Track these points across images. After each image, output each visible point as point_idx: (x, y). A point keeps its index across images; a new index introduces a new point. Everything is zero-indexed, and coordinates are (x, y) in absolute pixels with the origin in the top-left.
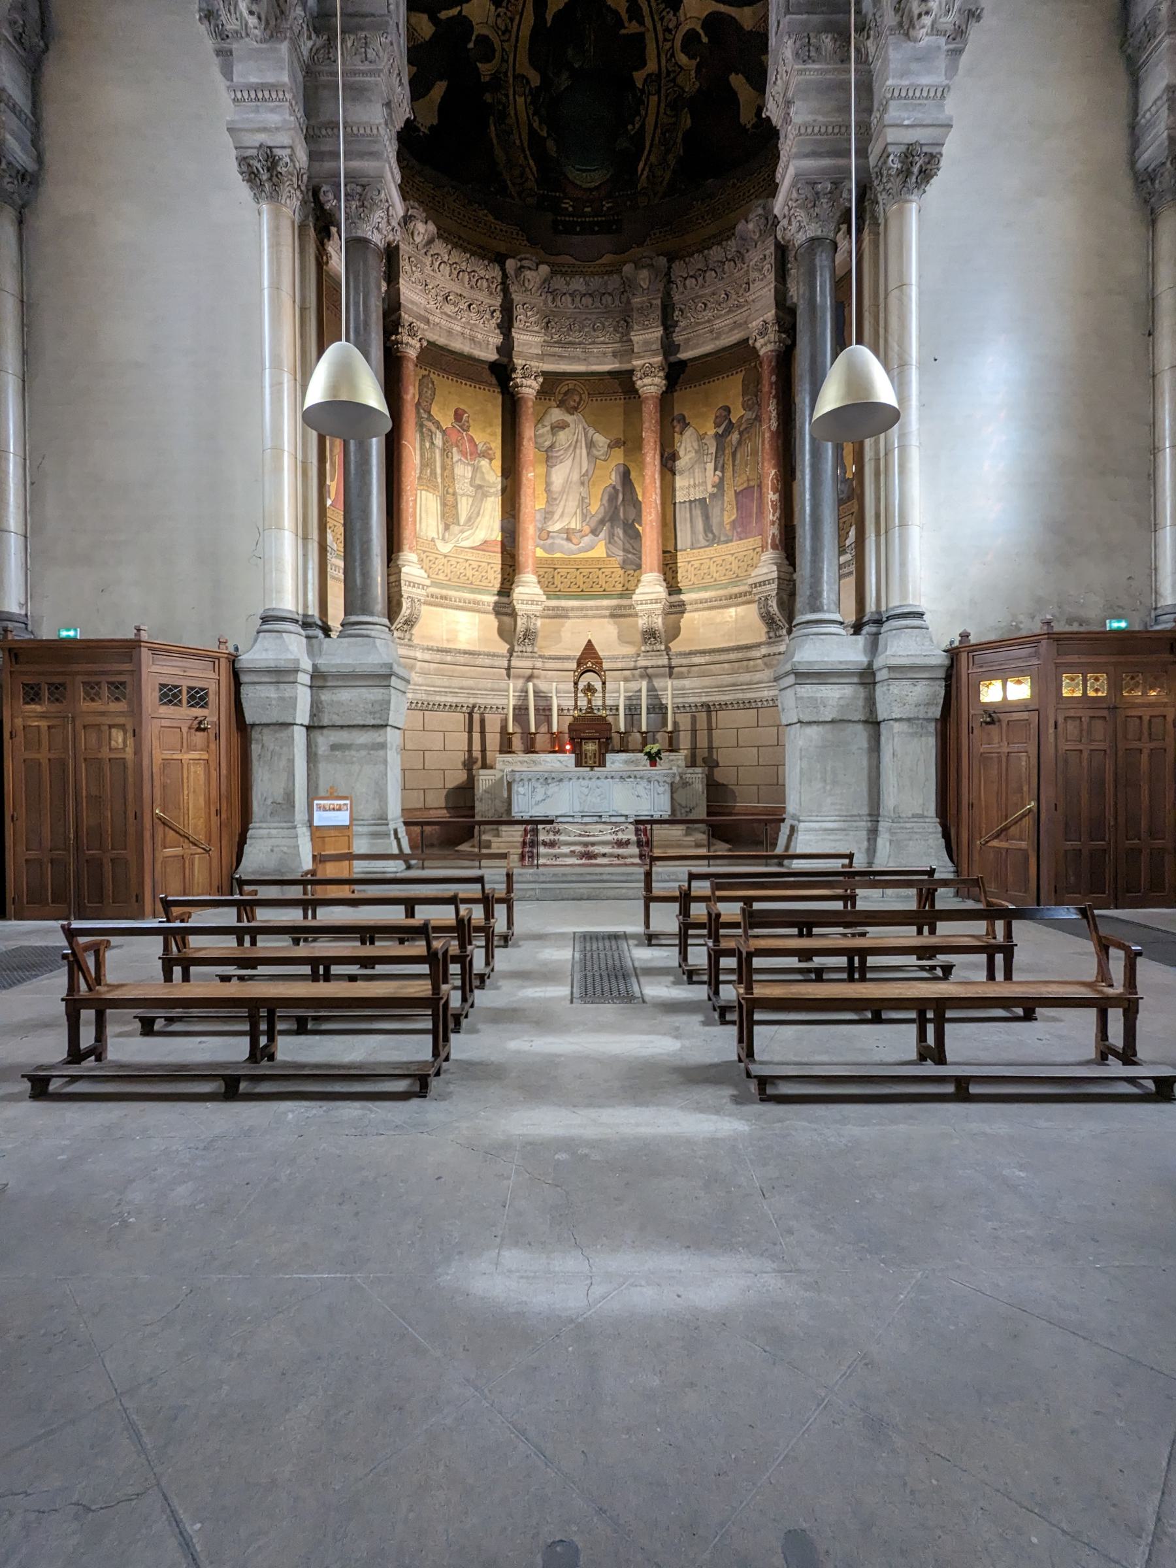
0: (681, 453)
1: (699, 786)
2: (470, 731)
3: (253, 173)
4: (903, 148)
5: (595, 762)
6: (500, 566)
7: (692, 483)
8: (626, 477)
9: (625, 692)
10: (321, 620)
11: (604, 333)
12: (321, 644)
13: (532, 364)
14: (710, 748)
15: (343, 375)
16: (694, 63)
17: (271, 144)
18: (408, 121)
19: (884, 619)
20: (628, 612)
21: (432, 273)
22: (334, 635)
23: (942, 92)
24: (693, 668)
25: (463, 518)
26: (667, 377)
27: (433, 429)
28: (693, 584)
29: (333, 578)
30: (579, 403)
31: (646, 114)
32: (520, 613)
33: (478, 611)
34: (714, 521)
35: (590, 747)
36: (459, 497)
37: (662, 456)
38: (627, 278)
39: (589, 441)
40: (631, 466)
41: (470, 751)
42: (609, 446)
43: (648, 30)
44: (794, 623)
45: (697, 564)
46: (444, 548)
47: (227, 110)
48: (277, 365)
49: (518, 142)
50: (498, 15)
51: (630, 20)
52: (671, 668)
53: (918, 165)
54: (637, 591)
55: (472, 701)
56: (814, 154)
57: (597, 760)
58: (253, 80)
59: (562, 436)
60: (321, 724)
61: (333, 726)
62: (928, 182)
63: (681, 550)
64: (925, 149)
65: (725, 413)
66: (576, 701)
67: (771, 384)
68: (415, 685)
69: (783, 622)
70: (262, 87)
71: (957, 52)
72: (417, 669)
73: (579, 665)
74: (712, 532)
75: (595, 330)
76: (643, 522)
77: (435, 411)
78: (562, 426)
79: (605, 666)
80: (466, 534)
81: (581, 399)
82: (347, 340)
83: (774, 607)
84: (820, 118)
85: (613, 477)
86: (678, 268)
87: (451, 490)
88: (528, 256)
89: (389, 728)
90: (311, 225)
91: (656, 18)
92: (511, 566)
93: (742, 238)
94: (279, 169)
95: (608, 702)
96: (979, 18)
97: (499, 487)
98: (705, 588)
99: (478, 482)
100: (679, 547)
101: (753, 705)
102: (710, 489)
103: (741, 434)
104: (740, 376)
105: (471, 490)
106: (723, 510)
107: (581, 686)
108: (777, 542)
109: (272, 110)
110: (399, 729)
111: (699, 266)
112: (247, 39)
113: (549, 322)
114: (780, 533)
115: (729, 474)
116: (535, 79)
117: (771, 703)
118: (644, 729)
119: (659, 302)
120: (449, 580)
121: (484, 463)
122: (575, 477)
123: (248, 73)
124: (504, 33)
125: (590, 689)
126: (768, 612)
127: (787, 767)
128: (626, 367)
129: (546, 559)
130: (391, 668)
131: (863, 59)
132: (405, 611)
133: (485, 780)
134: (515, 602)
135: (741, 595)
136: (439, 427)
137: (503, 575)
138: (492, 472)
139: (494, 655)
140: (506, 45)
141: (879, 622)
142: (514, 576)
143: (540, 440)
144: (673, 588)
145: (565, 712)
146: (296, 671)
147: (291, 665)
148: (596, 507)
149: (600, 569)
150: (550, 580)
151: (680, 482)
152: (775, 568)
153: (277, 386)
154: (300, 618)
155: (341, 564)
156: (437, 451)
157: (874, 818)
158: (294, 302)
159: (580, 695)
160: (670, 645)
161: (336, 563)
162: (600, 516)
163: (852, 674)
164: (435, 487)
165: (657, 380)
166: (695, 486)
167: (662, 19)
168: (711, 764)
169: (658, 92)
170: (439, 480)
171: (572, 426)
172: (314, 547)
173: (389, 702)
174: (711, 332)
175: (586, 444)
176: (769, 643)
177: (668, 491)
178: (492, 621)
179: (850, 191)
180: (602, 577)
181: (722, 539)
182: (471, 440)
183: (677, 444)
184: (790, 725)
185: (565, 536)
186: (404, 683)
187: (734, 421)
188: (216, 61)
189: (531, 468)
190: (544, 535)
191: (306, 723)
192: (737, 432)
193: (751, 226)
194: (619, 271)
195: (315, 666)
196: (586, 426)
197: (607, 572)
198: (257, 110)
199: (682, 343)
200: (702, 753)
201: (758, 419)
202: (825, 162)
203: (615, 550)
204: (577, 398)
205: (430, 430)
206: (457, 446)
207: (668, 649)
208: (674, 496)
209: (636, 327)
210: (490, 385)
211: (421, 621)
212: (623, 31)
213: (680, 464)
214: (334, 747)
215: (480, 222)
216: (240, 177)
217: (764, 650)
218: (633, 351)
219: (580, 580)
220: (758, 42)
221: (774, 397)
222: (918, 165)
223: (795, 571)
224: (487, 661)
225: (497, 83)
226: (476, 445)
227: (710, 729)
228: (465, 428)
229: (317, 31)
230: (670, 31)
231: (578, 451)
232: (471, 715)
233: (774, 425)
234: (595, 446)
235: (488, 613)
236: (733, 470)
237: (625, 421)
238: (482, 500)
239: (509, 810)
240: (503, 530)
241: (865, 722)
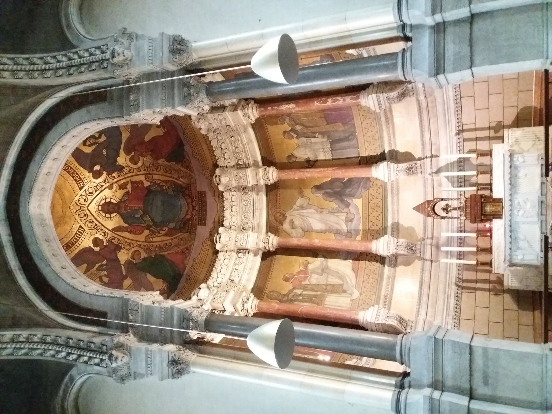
0: (306, 157)
1: (518, 133)
2: (476, 289)
3: (178, 372)
4: (171, 54)
5: (499, 206)
6: (367, 262)
7: (322, 150)
8: (318, 188)
9: (448, 187)
10: (399, 376)
11: (249, 200)
12: (414, 379)
13: (262, 238)
14: (490, 128)
15: (262, 340)
16: (141, 158)
17: (167, 361)
18: (161, 294)
19: (402, 23)
20: (395, 185)
21: (221, 287)
22: (408, 370)
23: (151, 39)
24: (433, 142)
25: (339, 281)
26: (269, 166)
27: (293, 294)
28: (379, 145)
29: (373, 364)
30: (281, 213)
31: (159, 180)
32: (395, 252)
33: (394, 277)
34: (342, 135)
35: (489, 209)
36: (328, 283)
37: (308, 168)
38: (225, 188)
39: (300, 208)
40: (313, 184)
41: (490, 290)
42: (302, 197)
43: (130, 180)
44: (404, 80)
45: (367, 144)
46: (356, 294)
47: (153, 379)
48: (259, 376)
49: (170, 241)
50: (124, 248)
51: (126, 188)
52: (432, 156)
53: (177, 46)
54: (383, 179)
55: (454, 287)
56: (173, 99)
57: (497, 204)
58: (144, 364)
59: (297, 223)
60: (469, 389)
61: (470, 381)
62: (184, 40)
63: (359, 154)
64: (171, 44)
65: (287, 134)
66: (454, 218)
67: (272, 109)
68: (442, 322)
69: (403, 87)
70: (147, 361)
71: (137, 36)
72: (432, 319)
73: (429, 216)
74: (349, 136)
75: (247, 205)
76: (343, 177)
77: (284, 292)
78: (292, 222)
79: (430, 198)
80: (348, 280)
81: (279, 213)
82: (246, 336)
83: (394, 94)
84: (160, 96)
85: (318, 195)
86: (221, 163)
87: (324, 287)
88: (215, 239)
89: (472, 344)
90: (199, 347)
91: (126, 176)
92: (367, 255)
93: (208, 131)
94: (177, 359)
95: (456, 197)
96: (125, 29)
97: (323, 259)
98: (381, 138)
99: (320, 271)
100: (357, 155)
101: (459, 101)
102: (325, 139)
103: (297, 124)
104: (269, 127)
105: (325, 275)
106: (337, 131)
107: (443, 214)
108: (355, 96)
109: (155, 358)
110: (472, 337)
111: (220, 152)
112: (130, 364)
113: (243, 228)
114: (351, 95)
115: (316, 129)
116: (147, 232)
117: (458, 89)
118: (475, 173)
119: (235, 172)
120: (375, 293)
121: (310, 267)
122: (318, 216)
123: (141, 367)
124: (130, 246)
125: (446, 209)
126: (398, 97)
127: (504, 73)
128: (264, 189)
129: (363, 234)
130: (430, 337)
131: (138, 80)
132: (394, 323)
133: (510, 282)
134: (389, 254)
135: (386, 116)
136: (291, 291)
137: (372, 261)
138: (316, 263)
139: (423, 270)
140: (135, 245)
141: (404, 26)
142: (373, 254)
143: (299, 235)
144: (381, 158)
145: (462, 225)
146: (431, 399)
147: (428, 401)
148: (334, 205)
149: (369, 202)
150: (375, 232)
151: (321, 157)
152: (370, 96)
153: (269, 378)
154: (398, 390)
155: (365, 359)
156: (305, 293)
157: (545, 6)
158: (231, 362)
159: (450, 215)
160: (417, 157)
161: (365, 362)
162: (339, 203)
163: (437, 37)
164: (323, 296)
165: (270, 172)
166: (323, 148)
167: (126, 174)
168: (499, 127)
169: (151, 174)
170: (319, 293)
171: (292, 217)
172: (355, 374)
173: (454, 342)
174: (248, 144)
175: (301, 210)
176: (417, 95)
177: (326, 164)
178: (400, 269)
179: (187, 78)
180: (373, 201)
181: (353, 130)
182: (299, 273)
183: (302, 160)
184: (473, 74)
185: (350, 223)
186: (440, 330)
187: (290, 128)
188: (138, 380)
189: (313, 241)
190: (349, 235)
191: (467, 399)
192: (296, 126)
193: (203, 127)
194: (222, 192)
195: (430, 386)
196: (292, 210)
197: (371, 198)
198: (155, 365)
199: (254, 159)
200: (492, 133)
201: (289, 115)
202: (176, 91)
203: (358, 193)
204: (279, 214)
205: (293, 296)
206: (301, 281)
207: (420, 159)
208: (329, 160)
209: (246, 184)
210: (272, 260)
211: (400, 314)
212: (130, 192)
213: (312, 158)
214: (486, 383)
215: (201, 262)
216: (180, 379)
217: (422, 97)
218: (257, 185)
219: (375, 214)
220: (134, 128)
221: (279, 107)
222: (177, 46)
223: (371, 84)
224: (427, 274)
225: (148, 249)
226: (301, 271)
227: (476, 129)
228: (292, 276)
229: (128, 332)
230: (130, 170)
231: (304, 214)
232: (463, 288)
233: (292, 106)
234: (302, 205)
235: (395, 271)
236: (316, 127)
237: (290, 189)
238: (330, 269)
239: (536, 267)
240: (346, 259)
241: (471, 24)
